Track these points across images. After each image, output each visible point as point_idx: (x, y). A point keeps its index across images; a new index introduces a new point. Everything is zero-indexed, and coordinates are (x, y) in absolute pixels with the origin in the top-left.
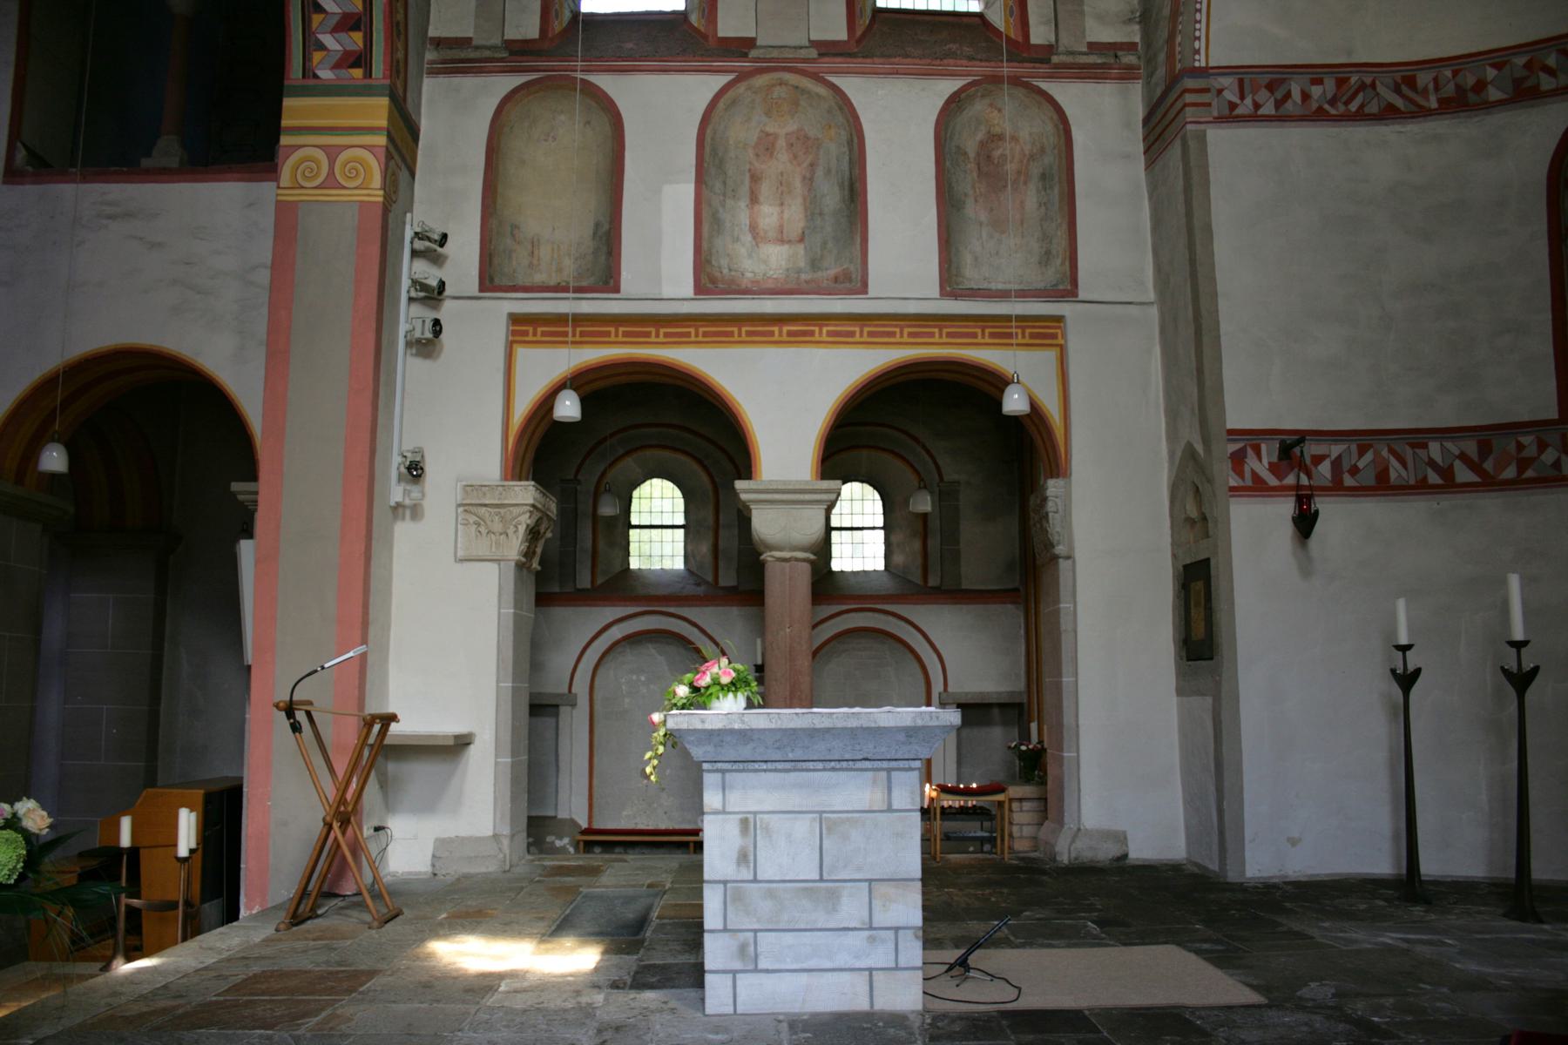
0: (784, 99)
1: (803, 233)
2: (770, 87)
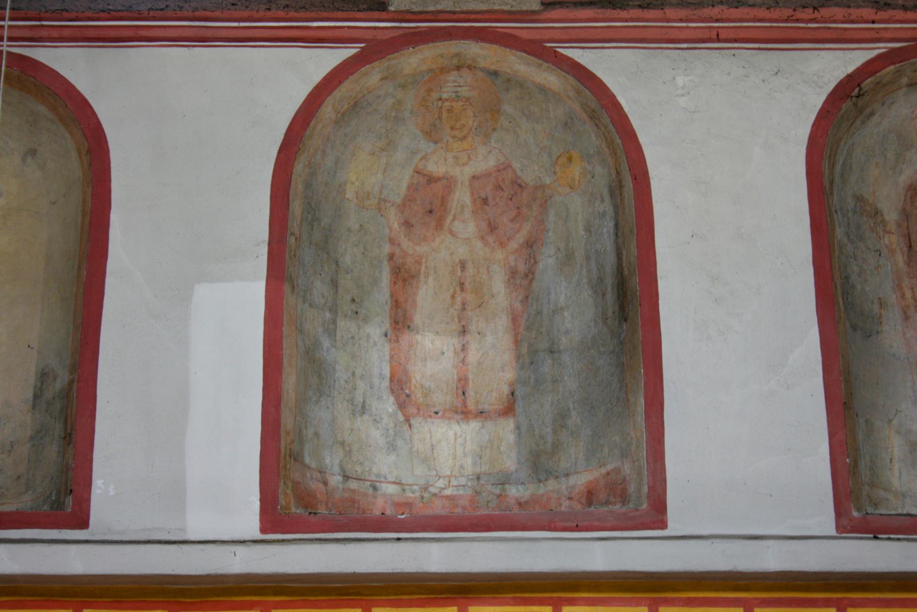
2: (439, 72)
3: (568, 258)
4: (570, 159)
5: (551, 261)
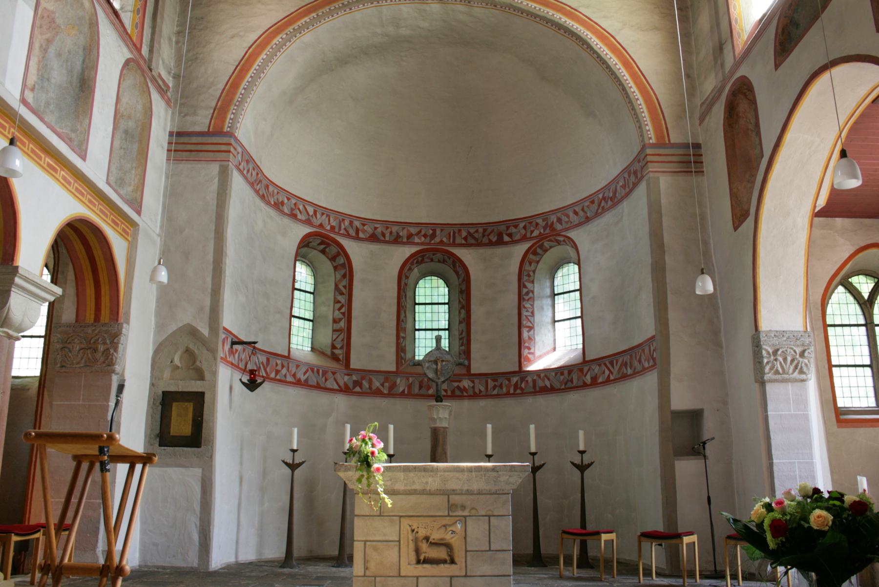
1: (34, 85)
3: (59, 55)
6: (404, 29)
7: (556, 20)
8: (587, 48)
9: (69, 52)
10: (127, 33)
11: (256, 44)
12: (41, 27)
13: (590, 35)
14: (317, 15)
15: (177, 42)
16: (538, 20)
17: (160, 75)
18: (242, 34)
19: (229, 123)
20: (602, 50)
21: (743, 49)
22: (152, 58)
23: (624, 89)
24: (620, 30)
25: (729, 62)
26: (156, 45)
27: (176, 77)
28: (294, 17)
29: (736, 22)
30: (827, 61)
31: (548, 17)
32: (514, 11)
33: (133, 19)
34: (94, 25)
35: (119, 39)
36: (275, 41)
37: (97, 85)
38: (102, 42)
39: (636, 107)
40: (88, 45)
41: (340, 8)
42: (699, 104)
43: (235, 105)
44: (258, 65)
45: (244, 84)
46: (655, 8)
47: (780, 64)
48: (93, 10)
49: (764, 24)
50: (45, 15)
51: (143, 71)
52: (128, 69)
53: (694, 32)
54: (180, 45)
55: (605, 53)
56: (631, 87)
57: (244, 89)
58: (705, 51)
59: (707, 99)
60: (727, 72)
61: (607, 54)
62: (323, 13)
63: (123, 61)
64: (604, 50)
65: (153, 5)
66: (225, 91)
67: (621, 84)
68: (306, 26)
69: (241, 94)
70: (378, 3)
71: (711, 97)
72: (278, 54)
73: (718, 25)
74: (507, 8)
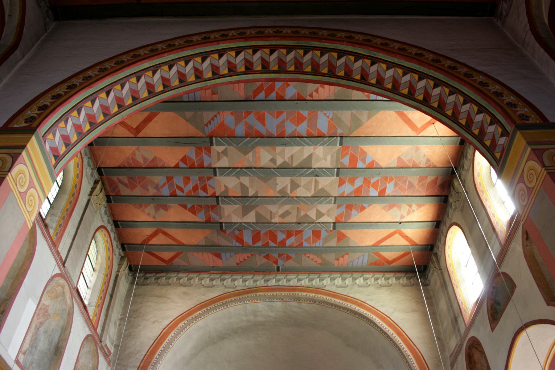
0: (57, 292)
1: (26, 351)
2: (60, 285)
3: (46, 332)
4: (58, 315)
5: (43, 330)
6: (260, 317)
7: (353, 309)
8: (374, 325)
9: (52, 330)
10: (90, 319)
11: (168, 327)
12: (38, 315)
13: (374, 317)
14: (207, 309)
15: (120, 325)
16: (342, 309)
17: (106, 345)
18: (160, 320)
19: (176, 331)
20: (383, 326)
21: (469, 320)
22: (103, 334)
23: (399, 349)
24: (392, 313)
25: (463, 329)
26: (106, 326)
27: (116, 346)
28: (192, 311)
29: (462, 304)
30: (522, 325)
31: (348, 308)
32: (327, 304)
33: (95, 310)
34: (70, 314)
35: (84, 323)
36: (180, 325)
37: (66, 351)
38: (74, 325)
39: (409, 360)
40: (65, 326)
41: (221, 305)
42: (449, 356)
43: (152, 365)
44: (169, 340)
45: (159, 352)
46: (412, 299)
47: (494, 328)
48: (72, 305)
49: (479, 304)
50: (43, 308)
51: (96, 343)
52: (87, 341)
53: (438, 312)
54: (121, 326)
55: (385, 327)
56: (404, 348)
57: (159, 355)
58: (447, 323)
59: (453, 352)
60: (462, 335)
61: (386, 328)
62: (210, 308)
63: (85, 336)
64: (384, 326)
65: (108, 303)
66: (146, 356)
67: (397, 346)
68: (200, 316)
69: (156, 358)
70: (244, 302)
71: (455, 351)
72: (182, 333)
73: (452, 307)
74: (323, 303)
